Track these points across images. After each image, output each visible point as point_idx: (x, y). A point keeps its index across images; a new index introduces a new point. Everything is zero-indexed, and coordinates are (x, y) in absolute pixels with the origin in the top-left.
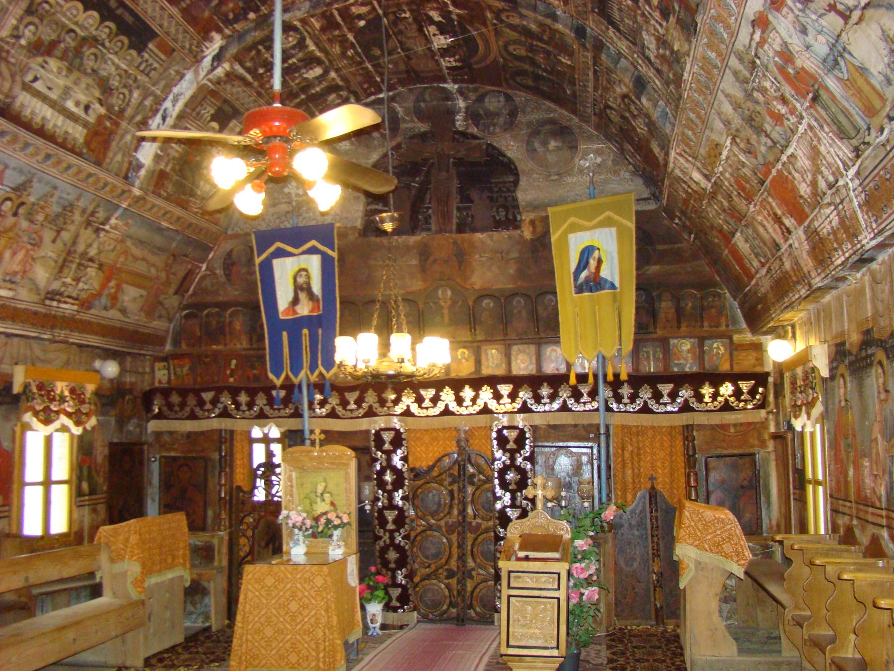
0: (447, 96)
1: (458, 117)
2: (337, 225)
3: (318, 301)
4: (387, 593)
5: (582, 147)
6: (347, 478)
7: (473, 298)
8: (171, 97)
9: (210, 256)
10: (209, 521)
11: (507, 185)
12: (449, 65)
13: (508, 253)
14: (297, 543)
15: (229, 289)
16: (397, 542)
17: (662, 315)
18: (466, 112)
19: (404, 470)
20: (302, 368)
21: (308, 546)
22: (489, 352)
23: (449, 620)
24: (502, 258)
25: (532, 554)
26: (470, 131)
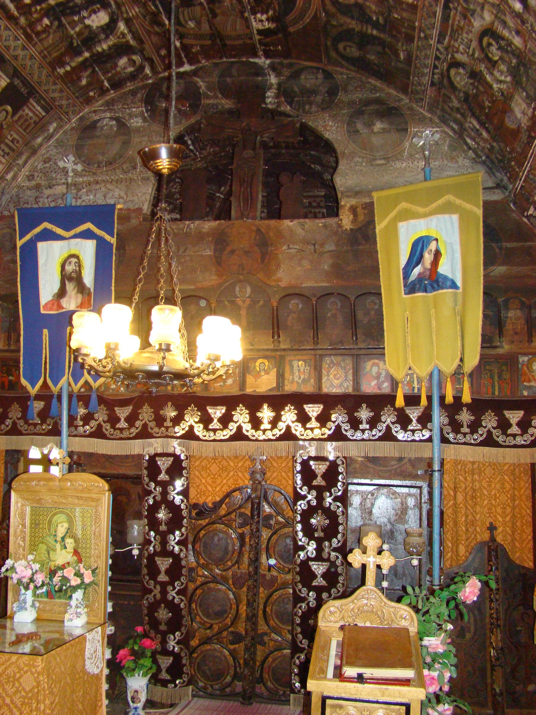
0: (258, 71)
1: (269, 94)
2: (119, 206)
3: (89, 294)
4: (155, 661)
6: (97, 518)
7: (277, 297)
11: (318, 200)
12: (261, 27)
13: (322, 245)
14: (22, 608)
17: (509, 327)
18: (279, 89)
19: (183, 506)
21: (39, 611)
22: (295, 363)
23: (233, 695)
24: (315, 251)
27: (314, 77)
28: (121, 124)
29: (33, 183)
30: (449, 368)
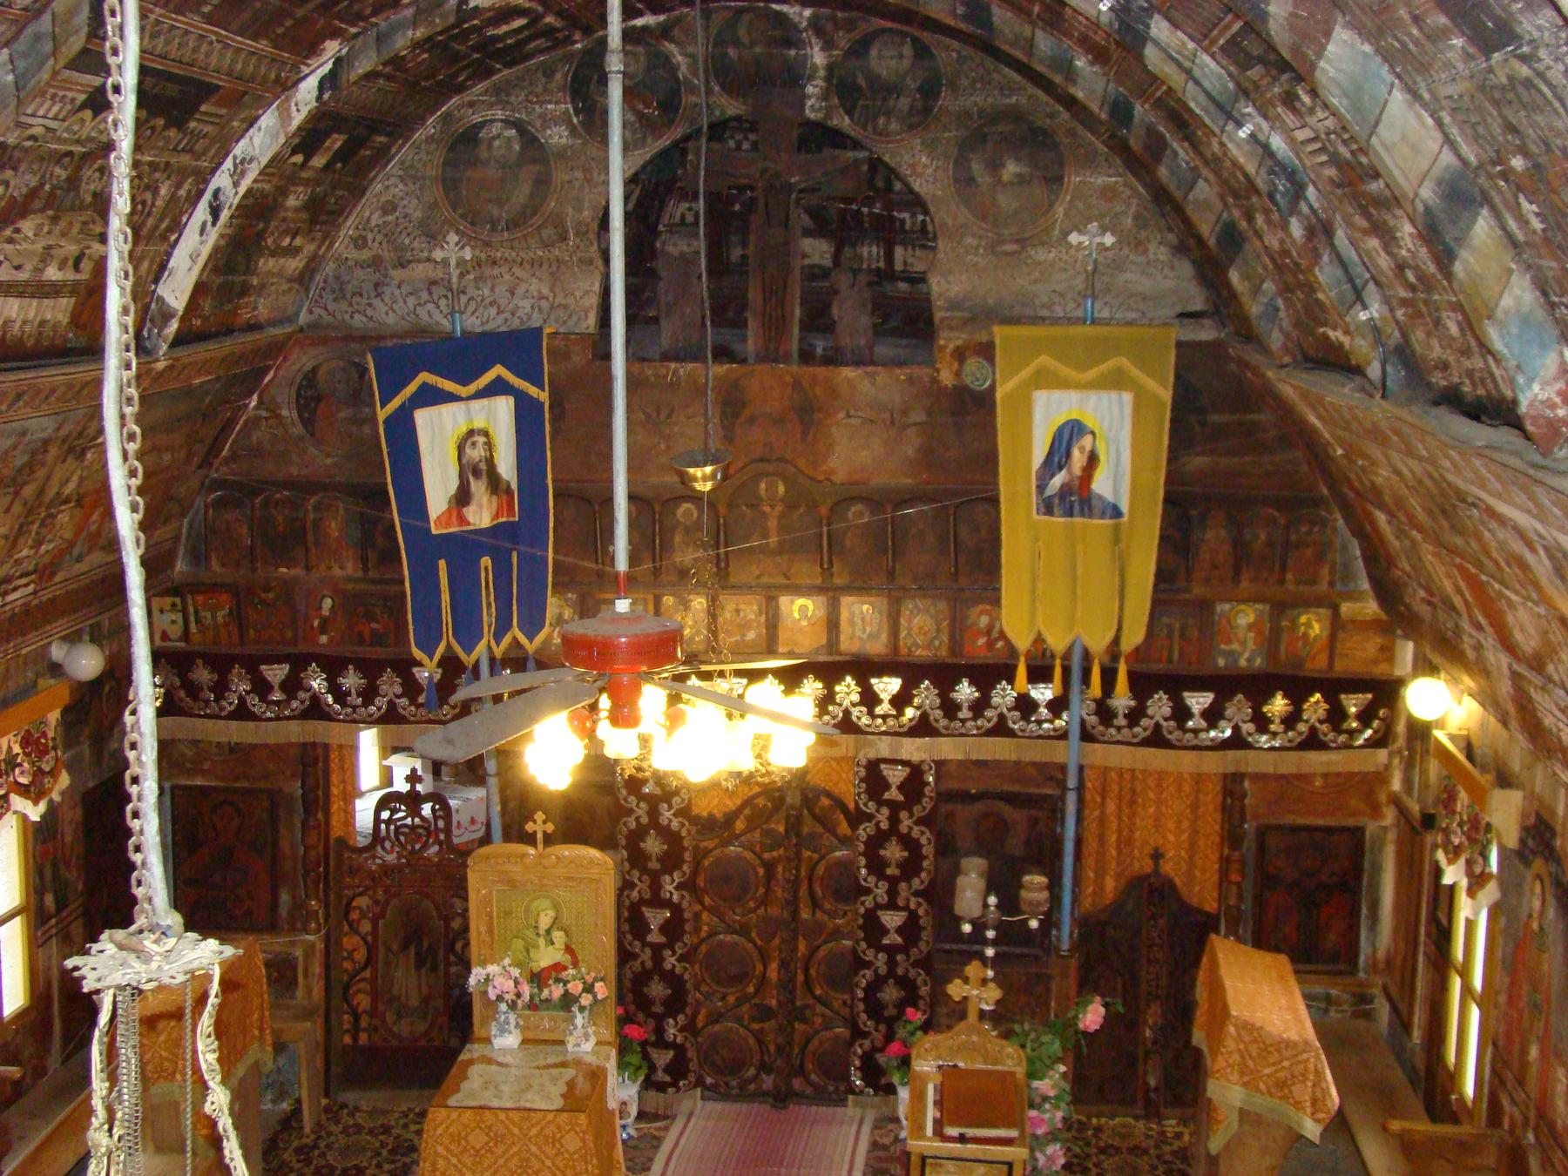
0: (787, 35)
2: (547, 330)
3: (509, 491)
4: (646, 1056)
5: (1074, 179)
7: (829, 503)
8: (228, 164)
9: (267, 379)
10: (284, 912)
13: (905, 412)
14: (503, 1031)
15: (312, 451)
16: (668, 966)
18: (828, 79)
20: (481, 637)
23: (760, 1096)
24: (893, 422)
25: (970, 1132)
26: (834, 122)
27: (893, 53)
28: (529, 140)
29: (366, 254)
30: (1098, 643)
